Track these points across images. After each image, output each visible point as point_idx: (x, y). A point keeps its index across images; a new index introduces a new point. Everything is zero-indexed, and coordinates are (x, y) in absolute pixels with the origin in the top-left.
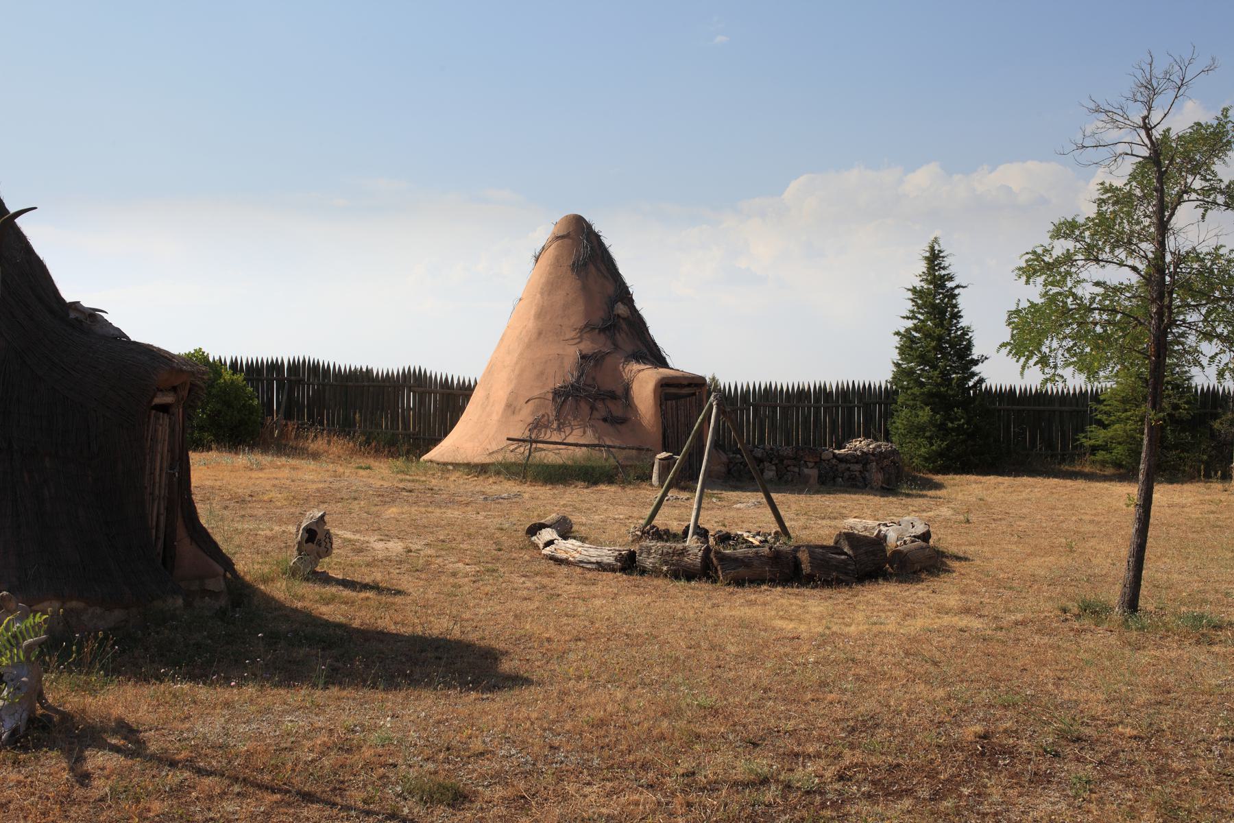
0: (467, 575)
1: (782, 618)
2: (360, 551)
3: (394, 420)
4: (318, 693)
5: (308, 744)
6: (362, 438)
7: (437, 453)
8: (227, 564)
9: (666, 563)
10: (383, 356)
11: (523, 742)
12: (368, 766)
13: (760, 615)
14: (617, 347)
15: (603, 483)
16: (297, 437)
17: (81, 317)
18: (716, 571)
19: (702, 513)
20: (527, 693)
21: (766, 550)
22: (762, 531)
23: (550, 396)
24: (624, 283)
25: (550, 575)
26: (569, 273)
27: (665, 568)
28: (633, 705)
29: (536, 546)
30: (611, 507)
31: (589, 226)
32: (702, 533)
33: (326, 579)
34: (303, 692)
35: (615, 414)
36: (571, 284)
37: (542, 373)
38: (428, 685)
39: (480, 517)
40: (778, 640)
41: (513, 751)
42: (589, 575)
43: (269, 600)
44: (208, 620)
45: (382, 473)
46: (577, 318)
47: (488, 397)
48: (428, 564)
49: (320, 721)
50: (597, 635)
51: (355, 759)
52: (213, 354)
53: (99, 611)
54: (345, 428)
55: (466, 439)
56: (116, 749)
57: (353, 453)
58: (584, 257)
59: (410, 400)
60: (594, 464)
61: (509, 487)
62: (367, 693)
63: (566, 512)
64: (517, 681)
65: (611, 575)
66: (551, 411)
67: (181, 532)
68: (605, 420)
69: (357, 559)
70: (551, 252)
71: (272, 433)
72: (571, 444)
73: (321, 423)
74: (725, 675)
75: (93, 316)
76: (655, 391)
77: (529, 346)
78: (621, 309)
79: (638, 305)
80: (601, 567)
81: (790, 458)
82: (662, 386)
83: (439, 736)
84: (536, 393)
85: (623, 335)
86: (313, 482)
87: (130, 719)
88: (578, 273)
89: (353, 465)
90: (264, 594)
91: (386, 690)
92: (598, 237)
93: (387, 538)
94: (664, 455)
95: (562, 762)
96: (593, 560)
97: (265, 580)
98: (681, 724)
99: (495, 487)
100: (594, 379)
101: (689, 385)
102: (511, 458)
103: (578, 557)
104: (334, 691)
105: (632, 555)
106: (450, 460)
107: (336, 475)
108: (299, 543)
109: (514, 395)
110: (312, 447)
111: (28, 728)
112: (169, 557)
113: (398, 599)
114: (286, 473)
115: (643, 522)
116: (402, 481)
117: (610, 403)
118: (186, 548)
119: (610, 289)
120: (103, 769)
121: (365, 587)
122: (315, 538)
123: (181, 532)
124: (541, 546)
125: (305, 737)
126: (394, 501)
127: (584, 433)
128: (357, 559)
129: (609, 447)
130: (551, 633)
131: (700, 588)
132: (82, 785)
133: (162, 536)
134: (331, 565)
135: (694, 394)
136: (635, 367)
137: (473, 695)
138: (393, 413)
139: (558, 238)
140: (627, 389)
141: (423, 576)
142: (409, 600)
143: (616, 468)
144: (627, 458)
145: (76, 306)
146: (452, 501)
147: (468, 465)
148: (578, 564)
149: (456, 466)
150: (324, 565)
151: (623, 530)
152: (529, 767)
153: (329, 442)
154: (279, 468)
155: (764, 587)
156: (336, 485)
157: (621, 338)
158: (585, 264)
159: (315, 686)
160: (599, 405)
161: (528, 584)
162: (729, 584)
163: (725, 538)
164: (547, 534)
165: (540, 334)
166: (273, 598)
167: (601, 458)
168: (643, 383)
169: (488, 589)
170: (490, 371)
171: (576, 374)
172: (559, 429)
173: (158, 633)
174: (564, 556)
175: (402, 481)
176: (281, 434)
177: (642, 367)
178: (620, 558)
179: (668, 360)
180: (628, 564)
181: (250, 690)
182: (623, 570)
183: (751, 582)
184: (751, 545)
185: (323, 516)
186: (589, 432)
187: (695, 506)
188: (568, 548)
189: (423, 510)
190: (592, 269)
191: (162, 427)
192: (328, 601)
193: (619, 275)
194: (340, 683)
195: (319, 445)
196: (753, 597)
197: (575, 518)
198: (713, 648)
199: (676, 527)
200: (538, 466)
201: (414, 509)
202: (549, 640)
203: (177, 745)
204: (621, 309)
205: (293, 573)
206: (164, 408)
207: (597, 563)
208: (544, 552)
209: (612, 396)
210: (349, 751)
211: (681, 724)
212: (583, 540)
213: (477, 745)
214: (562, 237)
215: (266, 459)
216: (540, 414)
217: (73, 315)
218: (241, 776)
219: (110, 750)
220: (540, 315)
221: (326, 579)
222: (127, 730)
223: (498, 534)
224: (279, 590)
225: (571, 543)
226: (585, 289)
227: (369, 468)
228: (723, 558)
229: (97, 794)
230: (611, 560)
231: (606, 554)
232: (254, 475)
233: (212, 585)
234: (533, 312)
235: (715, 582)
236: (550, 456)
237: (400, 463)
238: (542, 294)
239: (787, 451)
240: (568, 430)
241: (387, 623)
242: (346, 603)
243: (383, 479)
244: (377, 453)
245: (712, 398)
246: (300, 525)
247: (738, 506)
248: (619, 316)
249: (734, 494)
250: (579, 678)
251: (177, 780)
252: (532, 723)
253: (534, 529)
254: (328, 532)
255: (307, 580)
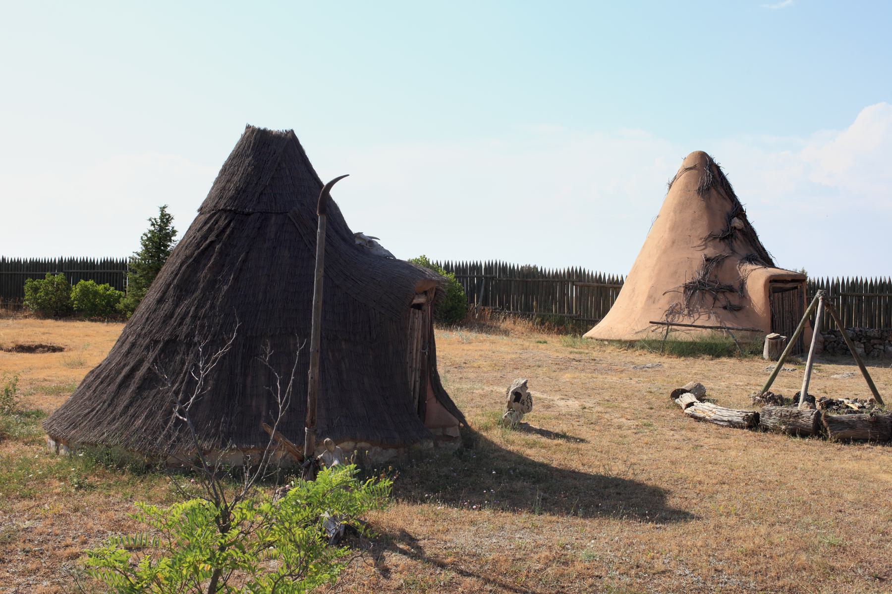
0: (630, 428)
1: (885, 472)
2: (548, 407)
3: (562, 307)
4: (535, 517)
5: (536, 557)
6: (538, 320)
7: (597, 331)
8: (461, 417)
9: (784, 423)
10: (552, 261)
11: (694, 565)
12: (581, 576)
13: (865, 468)
14: (734, 252)
15: (724, 356)
16: (491, 319)
17: (363, 243)
18: (826, 431)
19: (811, 381)
20: (692, 525)
21: (866, 415)
22: (859, 398)
23: (682, 290)
24: (739, 203)
25: (692, 429)
26: (696, 195)
27: (783, 427)
28: (776, 539)
29: (679, 407)
30: (732, 375)
31: (711, 160)
32: (811, 399)
33: (527, 429)
34: (524, 515)
35: (732, 303)
36: (697, 204)
37: (676, 272)
38: (614, 516)
39: (633, 382)
40: (886, 490)
41: (687, 572)
42: (723, 430)
43: (490, 443)
44: (448, 459)
45: (555, 346)
46: (702, 230)
47: (634, 290)
48: (599, 418)
49: (541, 539)
50: (737, 480)
51: (572, 571)
52: (433, 259)
53: (379, 449)
54: (525, 312)
55: (616, 322)
56: (404, 552)
57: (532, 330)
58: (710, 182)
59: (573, 292)
60: (717, 342)
61: (651, 358)
62: (569, 519)
63: (699, 379)
64: (680, 516)
65: (740, 431)
66: (682, 301)
67: (430, 394)
68: (725, 308)
69: (547, 413)
70: (681, 180)
71: (474, 315)
72: (700, 325)
73: (509, 309)
74: (847, 519)
75: (370, 242)
76: (765, 286)
77: (665, 252)
78: (737, 223)
79: (750, 219)
80: (732, 424)
81: (877, 338)
82: (770, 282)
83: (629, 556)
84: (671, 287)
85: (739, 242)
86: (508, 353)
87: (409, 529)
88: (703, 196)
89: (533, 340)
90: (486, 439)
91: (585, 517)
92: (718, 168)
93: (565, 397)
94: (773, 335)
95: (726, 583)
96: (725, 419)
97: (487, 429)
98: (817, 558)
99: (641, 358)
100: (716, 276)
101: (793, 281)
102: (653, 336)
103: (713, 416)
104: (547, 517)
105: (756, 416)
106: (606, 337)
107: (525, 349)
108: (509, 402)
109: (654, 289)
110: (503, 326)
111: (345, 533)
112: (422, 410)
113: (581, 446)
114: (487, 346)
115: (761, 389)
116: (571, 353)
117: (728, 295)
118: (433, 405)
119: (728, 207)
120: (397, 566)
121: (557, 436)
122: (520, 399)
123: (430, 394)
124: (684, 407)
125: (532, 551)
126: (567, 368)
127: (709, 318)
128: (547, 413)
129: (729, 328)
130: (701, 477)
131: (814, 444)
132: (385, 577)
133: (417, 396)
134: (530, 419)
135: (796, 288)
136: (748, 267)
137: (650, 525)
138: (566, 302)
139: (687, 169)
140: (742, 284)
141: (597, 428)
142: (589, 446)
143: (735, 345)
144: (742, 338)
145: (359, 235)
146: (610, 369)
147: (619, 341)
148: (713, 421)
149: (611, 342)
150: (528, 418)
151: (745, 395)
152: (701, 585)
153: (515, 323)
154: (481, 342)
155: (867, 445)
156: (524, 356)
157: (737, 245)
158: (708, 189)
159: (533, 512)
160: (720, 296)
161: (677, 437)
162: (837, 442)
163: (829, 404)
164: (688, 398)
165: (673, 243)
166: (493, 442)
167: (721, 337)
168: (755, 279)
169: (646, 439)
170: (635, 270)
171: (702, 273)
172: (689, 315)
173: (418, 466)
174: (702, 415)
175: (571, 353)
176: (481, 317)
177: (754, 267)
178: (747, 418)
179: (774, 261)
180: (754, 423)
181: (487, 512)
182: (750, 427)
183: (856, 440)
184: (852, 412)
185: (525, 383)
186: (713, 317)
187: (805, 378)
188: (704, 409)
189: (590, 375)
190: (714, 192)
191: (417, 320)
192: (532, 445)
193: (735, 196)
194: (550, 510)
195: (507, 324)
196: (858, 453)
197: (707, 384)
198: (832, 495)
199: (789, 394)
200: (674, 342)
201: (583, 375)
202: (700, 483)
203: (444, 552)
204: (737, 223)
205: (504, 423)
206: (419, 306)
207: (729, 421)
208: (686, 411)
209: (731, 289)
210: (566, 563)
211: (817, 558)
212: (714, 402)
213: (659, 565)
214: (690, 169)
215: (473, 335)
216: (674, 303)
217: (358, 242)
218: (492, 579)
219: (400, 553)
220: (673, 228)
221: (527, 429)
222: (411, 539)
223: (649, 396)
224: (496, 436)
225: (707, 405)
226: (709, 208)
227: (545, 342)
228: (831, 421)
229: (396, 584)
230: (740, 420)
231: (736, 415)
232: (466, 347)
233: (451, 432)
234: (668, 226)
235: (825, 439)
236: (683, 335)
237: (568, 338)
238: (675, 212)
239: (874, 332)
240: (696, 316)
241: (575, 464)
242: (545, 448)
243: (557, 351)
244: (550, 330)
245: (818, 294)
246: (509, 389)
247: (835, 376)
248: (735, 228)
249: (831, 366)
250: (728, 515)
251: (448, 578)
252: (699, 550)
253: (677, 394)
254: (529, 394)
255: (514, 429)
